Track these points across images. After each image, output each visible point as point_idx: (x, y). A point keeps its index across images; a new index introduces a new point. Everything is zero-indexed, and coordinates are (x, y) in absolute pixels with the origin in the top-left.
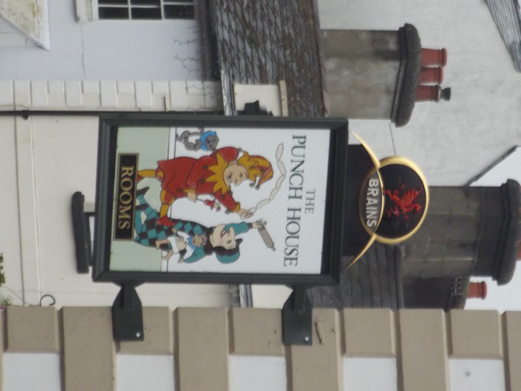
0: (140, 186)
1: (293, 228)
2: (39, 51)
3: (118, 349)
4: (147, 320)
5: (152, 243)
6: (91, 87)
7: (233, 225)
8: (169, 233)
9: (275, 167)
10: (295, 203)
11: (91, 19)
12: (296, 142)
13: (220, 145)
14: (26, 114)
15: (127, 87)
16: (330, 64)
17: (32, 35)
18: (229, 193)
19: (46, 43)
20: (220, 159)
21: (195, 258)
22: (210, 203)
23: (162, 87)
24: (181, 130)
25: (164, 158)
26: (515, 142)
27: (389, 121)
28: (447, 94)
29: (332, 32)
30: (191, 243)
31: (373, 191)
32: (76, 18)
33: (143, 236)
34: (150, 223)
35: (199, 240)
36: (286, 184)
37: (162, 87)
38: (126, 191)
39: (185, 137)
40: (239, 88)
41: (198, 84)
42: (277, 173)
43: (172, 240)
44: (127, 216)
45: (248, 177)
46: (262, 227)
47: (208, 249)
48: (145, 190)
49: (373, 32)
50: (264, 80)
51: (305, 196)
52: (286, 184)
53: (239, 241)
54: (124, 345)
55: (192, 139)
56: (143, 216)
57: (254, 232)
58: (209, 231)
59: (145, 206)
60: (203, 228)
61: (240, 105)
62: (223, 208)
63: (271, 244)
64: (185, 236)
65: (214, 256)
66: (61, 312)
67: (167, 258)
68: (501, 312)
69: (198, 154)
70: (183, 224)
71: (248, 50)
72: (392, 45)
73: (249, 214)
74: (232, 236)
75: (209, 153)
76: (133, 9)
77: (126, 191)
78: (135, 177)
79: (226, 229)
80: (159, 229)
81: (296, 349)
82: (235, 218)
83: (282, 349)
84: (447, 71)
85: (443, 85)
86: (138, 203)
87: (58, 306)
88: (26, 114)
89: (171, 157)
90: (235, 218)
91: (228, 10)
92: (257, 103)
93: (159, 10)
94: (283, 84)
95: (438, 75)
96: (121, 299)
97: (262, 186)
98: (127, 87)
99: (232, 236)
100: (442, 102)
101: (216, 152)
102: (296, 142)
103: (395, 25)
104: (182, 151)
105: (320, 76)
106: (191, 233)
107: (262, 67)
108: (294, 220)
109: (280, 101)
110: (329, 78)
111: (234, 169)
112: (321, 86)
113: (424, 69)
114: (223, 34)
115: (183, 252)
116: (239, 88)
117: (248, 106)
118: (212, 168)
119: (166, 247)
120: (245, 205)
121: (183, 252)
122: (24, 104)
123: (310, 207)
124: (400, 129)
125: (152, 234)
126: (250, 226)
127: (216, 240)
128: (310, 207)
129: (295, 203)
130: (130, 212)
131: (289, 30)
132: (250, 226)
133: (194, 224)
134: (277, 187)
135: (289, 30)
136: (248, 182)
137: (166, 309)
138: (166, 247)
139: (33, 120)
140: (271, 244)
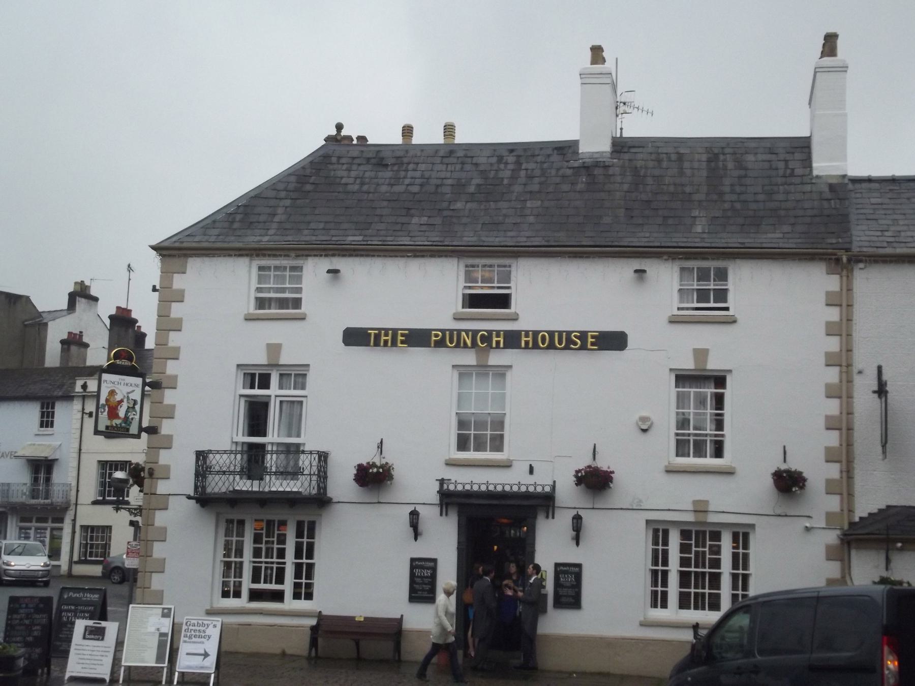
0: (114, 425)
1: (129, 385)
2: (62, 445)
3: (160, 433)
4: (152, 425)
5: (131, 423)
6: (74, 431)
7: (127, 400)
8: (128, 418)
9: (112, 389)
10: (122, 384)
11: (53, 430)
12: (105, 383)
13: (105, 403)
14: (80, 450)
15: (74, 421)
16: (70, 364)
17: (57, 447)
18: (118, 401)
19: (59, 443)
20: (108, 403)
21: (136, 412)
22: (121, 406)
23: (75, 412)
24: (100, 413)
25: (107, 418)
26: (96, 315)
27: (88, 349)
28: (81, 332)
29: (61, 363)
30: (132, 412)
31: (120, 363)
32: (53, 434)
33: (129, 425)
34: (125, 423)
35: (131, 410)
36: (117, 386)
37: (75, 412)
38: (115, 429)
39: (102, 412)
40: (77, 390)
41: (75, 401)
42: (114, 388)
43: (130, 417)
44: (417, 586)
45: (114, 396)
46: (128, 393)
47: (133, 408)
48: (116, 424)
49: (62, 352)
50: (75, 383)
51: (120, 381)
52: (117, 386)
53: (132, 399)
54: (159, 431)
55: (103, 410)
56: (123, 425)
57: (130, 395)
58: (129, 408)
59: (121, 424)
60: (128, 409)
61: (82, 390)
62: (122, 403)
63: (133, 391)
64: (129, 414)
65: (136, 406)
66: (148, 448)
67: (136, 419)
68: (156, 331)
69: (107, 409)
70: (126, 414)
71: (65, 387)
72: (66, 346)
73: (125, 396)
74: (131, 401)
75: (107, 406)
76: (306, 579)
77: (115, 429)
78: (112, 426)
79: (128, 403)
80: (127, 421)
81: (163, 386)
82: (125, 400)
83: (163, 389)
84: (74, 332)
85: (79, 333)
86: (119, 426)
87: (147, 448)
88: (80, 450)
89: (107, 416)
90: (125, 400)
91: (53, 392)
92: (82, 386)
93: (307, 564)
94: (76, 378)
95: (75, 335)
96: (146, 432)
97: (117, 392)
98: (74, 421)
99: (131, 401)
100: (83, 334)
101: (106, 404)
102: (105, 383)
103: (60, 345)
104: (106, 413)
105: (74, 367)
106: (129, 412)
107: (71, 384)
108: (127, 384)
109: (81, 379)
110: (74, 365)
111: (112, 400)
112: (78, 368)
113: (74, 338)
114: (60, 394)
115: (134, 415)
116: (77, 390)
117: (82, 388)
118: (111, 405)
119: (132, 419)
120: (122, 397)
121: (134, 415)
122: (77, 450)
123: (124, 380)
124: (91, 345)
125: (128, 422)
126: (128, 396)
127: (131, 406)
128: (124, 380)
129: (122, 384)
130: (122, 428)
131: (60, 375)
132: (128, 396)
133: (126, 411)
134: (118, 388)
135: (60, 375)
136: (116, 396)
137: (150, 420)
138: (132, 419)
139: (82, 448)
140: (133, 391)
